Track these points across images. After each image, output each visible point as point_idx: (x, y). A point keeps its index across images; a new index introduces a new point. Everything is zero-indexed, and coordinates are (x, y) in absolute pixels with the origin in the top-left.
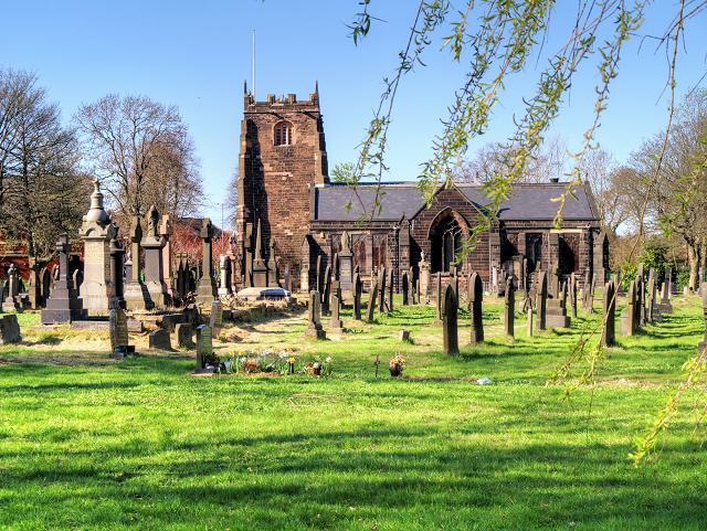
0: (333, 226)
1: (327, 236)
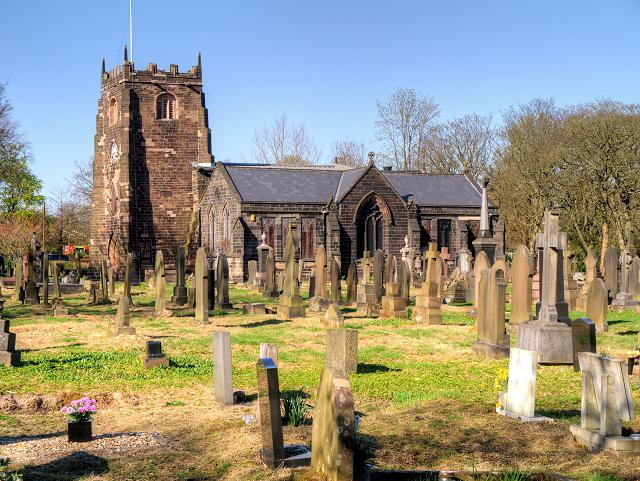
0: (263, 208)
1: (258, 219)
